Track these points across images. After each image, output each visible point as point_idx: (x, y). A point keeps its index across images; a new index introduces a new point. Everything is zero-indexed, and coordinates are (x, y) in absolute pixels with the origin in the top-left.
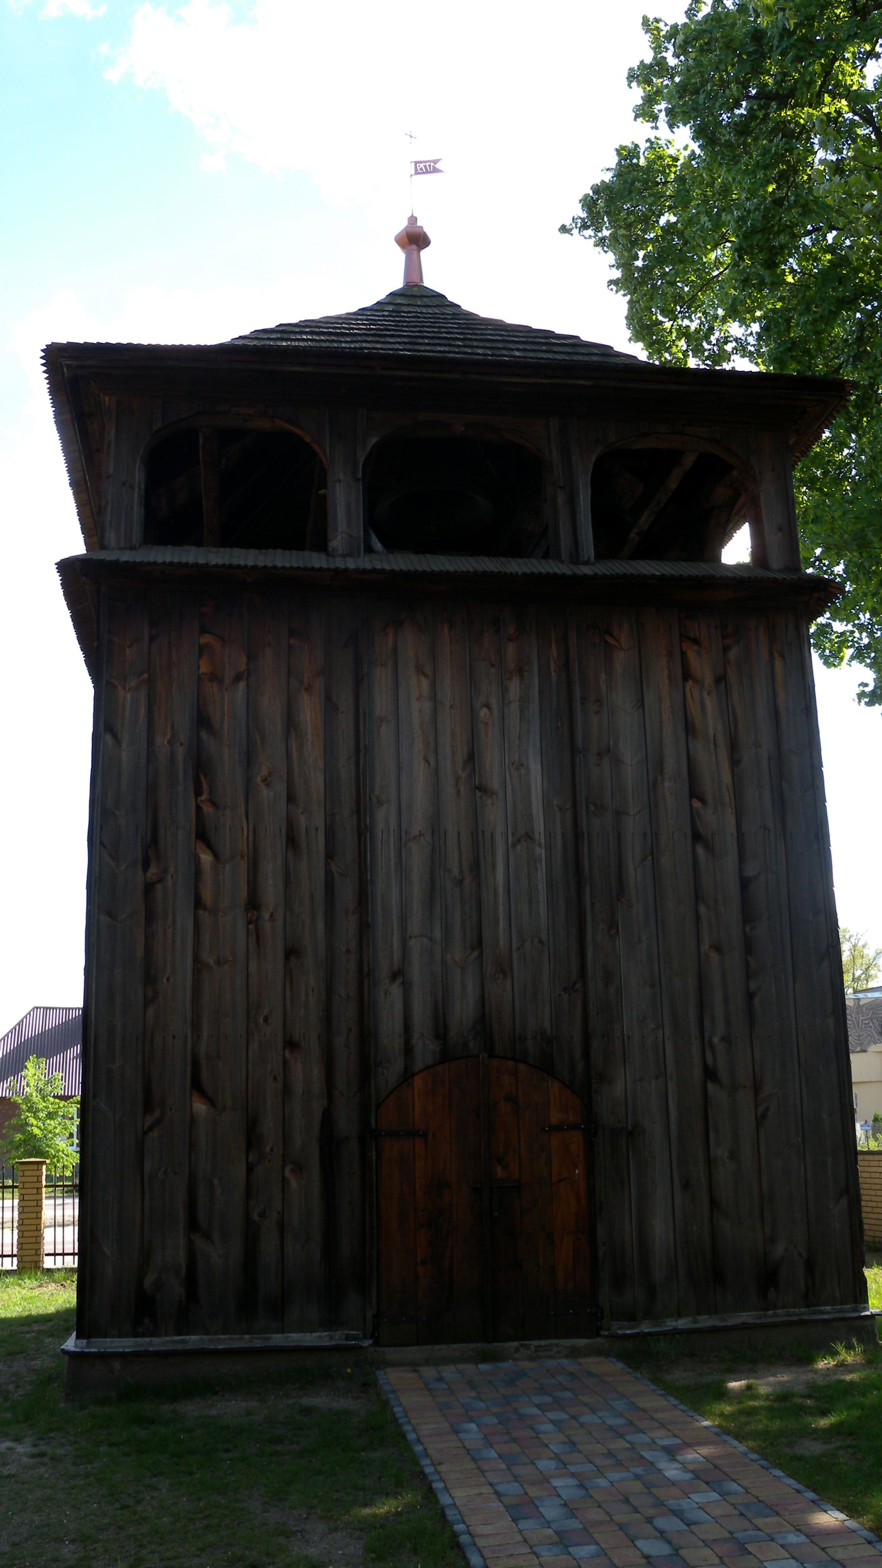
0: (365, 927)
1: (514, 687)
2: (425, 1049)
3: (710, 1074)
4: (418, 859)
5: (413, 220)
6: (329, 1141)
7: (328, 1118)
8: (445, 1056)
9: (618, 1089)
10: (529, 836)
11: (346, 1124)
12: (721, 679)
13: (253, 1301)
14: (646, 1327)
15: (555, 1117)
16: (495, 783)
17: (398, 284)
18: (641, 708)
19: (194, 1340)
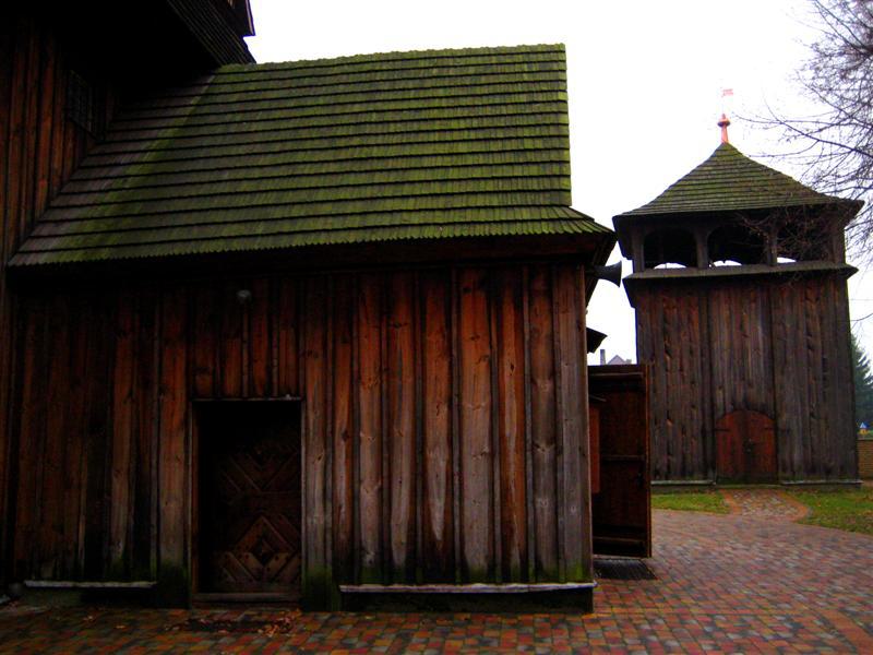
0: (712, 375)
1: (753, 305)
2: (730, 407)
3: (812, 415)
4: (726, 357)
5: (724, 116)
6: (703, 432)
7: (704, 426)
8: (735, 410)
9: (784, 419)
10: (758, 349)
11: (708, 428)
12: (817, 299)
13: (684, 473)
14: (792, 482)
15: (766, 426)
16: (748, 333)
17: (717, 144)
18: (794, 314)
19: (670, 482)
